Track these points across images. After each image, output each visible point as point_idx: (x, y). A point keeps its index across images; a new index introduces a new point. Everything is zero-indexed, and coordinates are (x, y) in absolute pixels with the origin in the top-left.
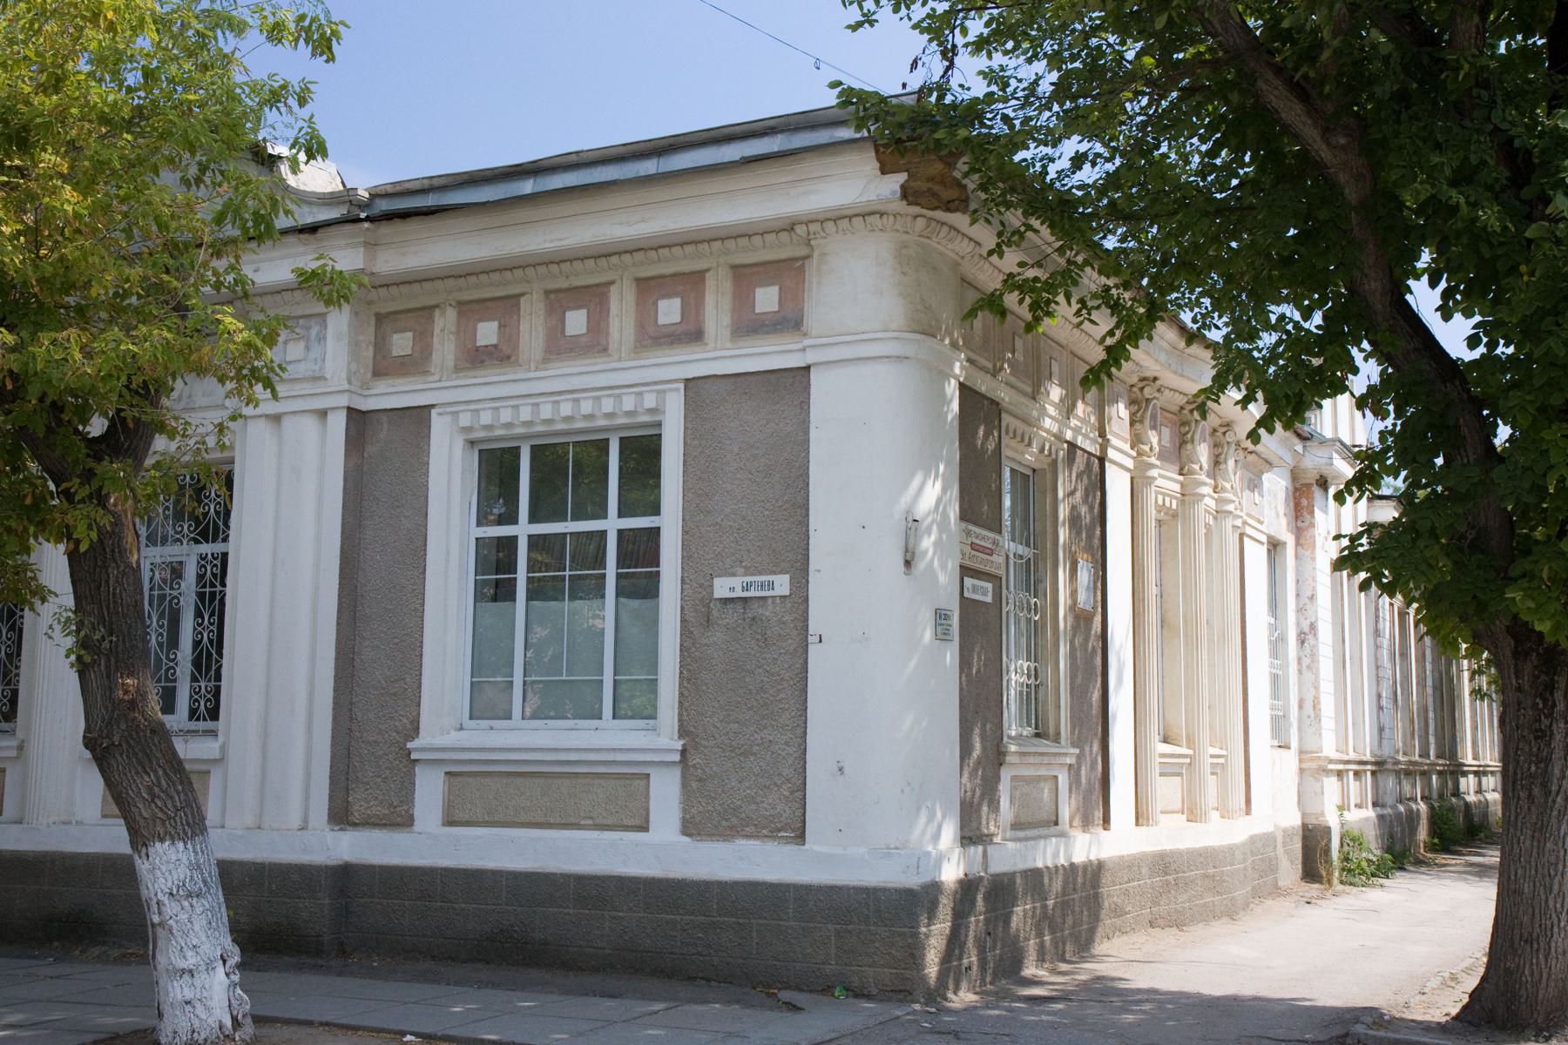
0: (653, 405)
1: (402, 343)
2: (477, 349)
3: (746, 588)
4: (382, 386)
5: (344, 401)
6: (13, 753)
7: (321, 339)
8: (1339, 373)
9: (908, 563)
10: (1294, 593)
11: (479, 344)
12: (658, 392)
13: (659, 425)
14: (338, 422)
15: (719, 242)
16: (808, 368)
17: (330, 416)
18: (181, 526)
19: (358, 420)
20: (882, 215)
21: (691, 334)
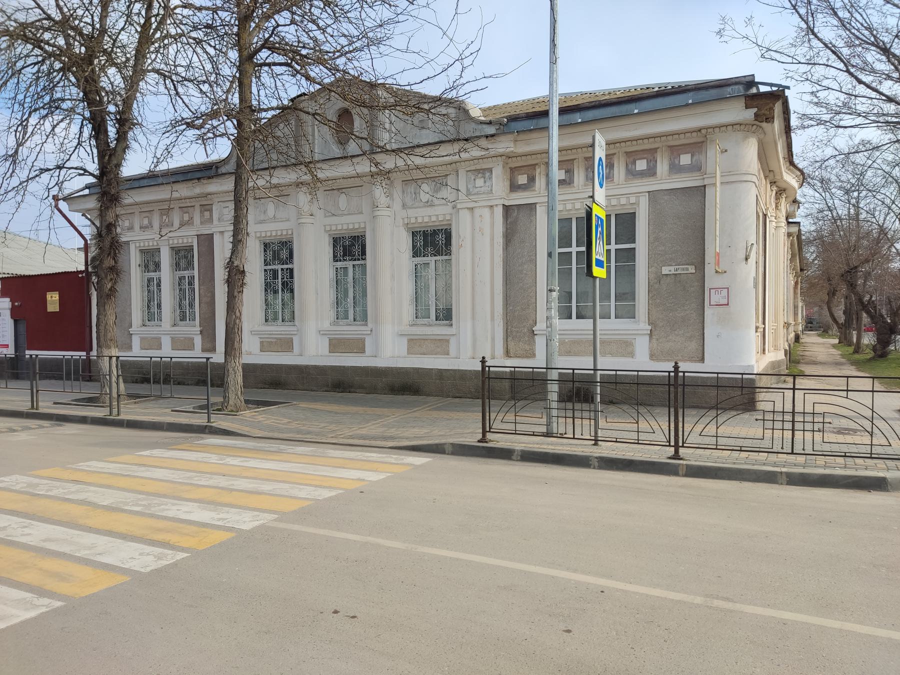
0: (363, 226)
1: (522, 179)
5: (502, 202)
6: (369, 332)
7: (491, 178)
12: (636, 196)
13: (450, 225)
14: (499, 211)
15: (665, 137)
16: (705, 186)
17: (495, 208)
18: (428, 249)
19: (507, 209)
20: (741, 125)
21: (651, 172)
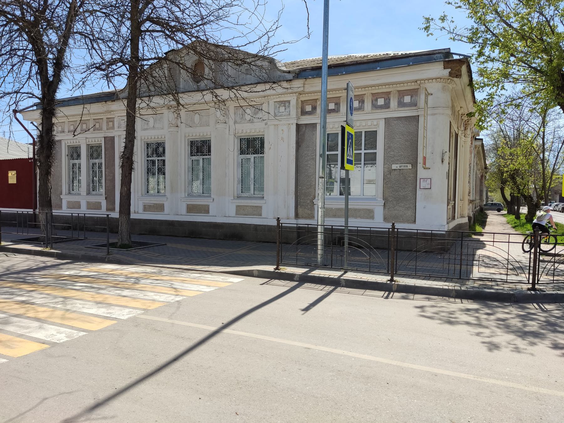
2: (329, 110)
3: (401, 167)
4: (304, 117)
6: (166, 200)
8: (21, 24)
9: (442, 162)
10: (82, 169)
11: (329, 109)
14: (294, 128)
16: (418, 116)
19: (298, 126)
